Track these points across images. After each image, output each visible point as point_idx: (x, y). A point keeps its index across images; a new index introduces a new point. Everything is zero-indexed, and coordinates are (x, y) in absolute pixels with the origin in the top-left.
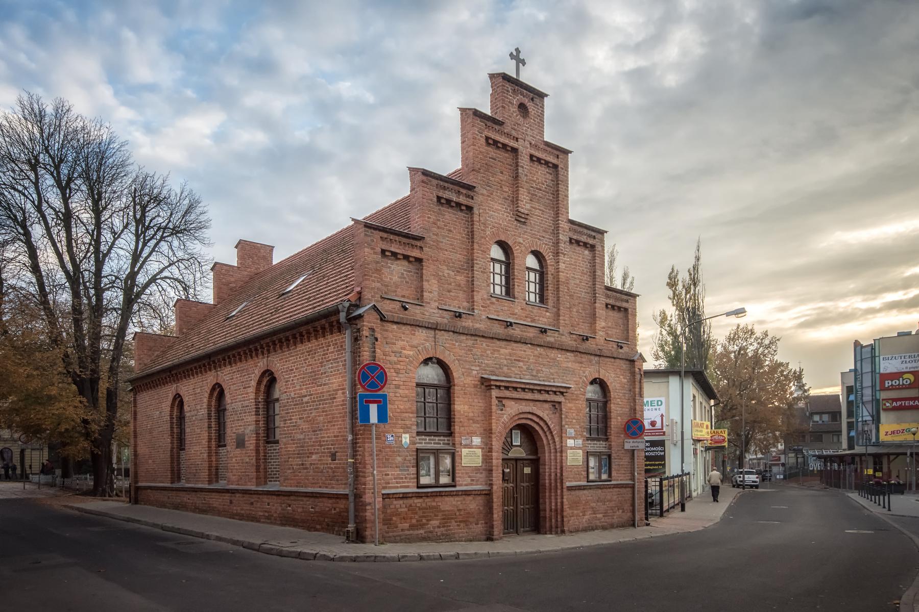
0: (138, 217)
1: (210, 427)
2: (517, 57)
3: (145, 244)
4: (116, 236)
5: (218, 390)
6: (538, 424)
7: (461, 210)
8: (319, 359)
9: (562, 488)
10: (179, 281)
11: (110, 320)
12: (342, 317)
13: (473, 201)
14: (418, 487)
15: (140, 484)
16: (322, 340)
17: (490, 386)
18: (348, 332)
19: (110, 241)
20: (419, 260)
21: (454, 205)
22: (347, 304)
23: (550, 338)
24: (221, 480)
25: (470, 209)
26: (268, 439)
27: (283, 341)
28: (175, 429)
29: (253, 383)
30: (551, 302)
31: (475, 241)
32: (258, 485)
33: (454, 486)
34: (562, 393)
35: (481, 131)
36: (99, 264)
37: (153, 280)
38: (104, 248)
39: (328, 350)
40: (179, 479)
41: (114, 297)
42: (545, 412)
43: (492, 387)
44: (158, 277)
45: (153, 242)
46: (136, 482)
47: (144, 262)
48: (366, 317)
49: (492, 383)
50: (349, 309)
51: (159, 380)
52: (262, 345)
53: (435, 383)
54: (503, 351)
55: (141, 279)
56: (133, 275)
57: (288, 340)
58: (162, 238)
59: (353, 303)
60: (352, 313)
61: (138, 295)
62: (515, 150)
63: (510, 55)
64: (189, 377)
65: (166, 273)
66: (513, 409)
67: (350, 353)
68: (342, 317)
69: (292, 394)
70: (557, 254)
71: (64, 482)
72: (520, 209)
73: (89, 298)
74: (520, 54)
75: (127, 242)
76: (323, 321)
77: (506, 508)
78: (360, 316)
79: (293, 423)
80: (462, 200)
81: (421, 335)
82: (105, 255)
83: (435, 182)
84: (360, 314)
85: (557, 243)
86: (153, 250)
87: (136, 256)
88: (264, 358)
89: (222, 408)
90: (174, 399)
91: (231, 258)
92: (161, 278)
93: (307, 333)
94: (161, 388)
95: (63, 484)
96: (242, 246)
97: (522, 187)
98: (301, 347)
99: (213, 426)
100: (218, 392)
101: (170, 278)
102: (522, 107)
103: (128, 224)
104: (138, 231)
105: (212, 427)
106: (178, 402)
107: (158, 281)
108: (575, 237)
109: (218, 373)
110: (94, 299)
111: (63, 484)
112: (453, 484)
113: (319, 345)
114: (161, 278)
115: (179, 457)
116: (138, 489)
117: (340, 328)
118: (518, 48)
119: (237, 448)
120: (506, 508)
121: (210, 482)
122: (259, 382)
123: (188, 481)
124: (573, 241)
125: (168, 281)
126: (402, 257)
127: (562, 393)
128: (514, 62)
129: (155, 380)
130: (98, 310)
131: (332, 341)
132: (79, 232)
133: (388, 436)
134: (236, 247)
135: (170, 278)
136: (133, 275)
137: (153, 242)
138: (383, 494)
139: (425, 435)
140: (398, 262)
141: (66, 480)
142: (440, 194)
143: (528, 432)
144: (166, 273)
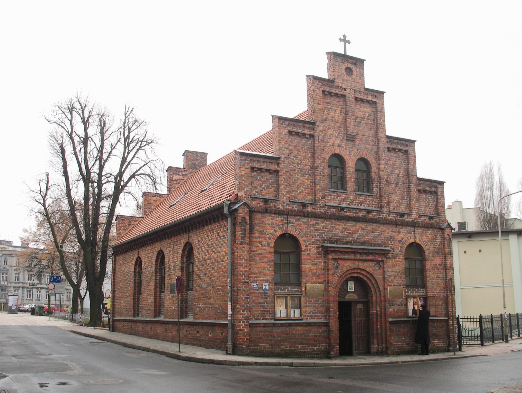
0: (126, 136)
1: (156, 279)
2: (344, 40)
3: (128, 153)
4: (113, 148)
5: (161, 254)
6: (366, 276)
7: (307, 138)
8: (216, 236)
9: (386, 323)
10: (149, 176)
11: (105, 205)
12: (226, 210)
13: (314, 131)
14: (275, 320)
15: (117, 318)
16: (217, 224)
17: (328, 251)
18: (229, 220)
19: (109, 150)
20: (277, 172)
21: (301, 135)
22: (228, 203)
23: (375, 216)
24: (162, 315)
25: (312, 136)
26: (189, 287)
27: (174, 231)
28: (137, 280)
29: (180, 251)
30: (376, 190)
31: (316, 156)
32: (134, 316)
33: (302, 320)
34: (384, 254)
35: (319, 88)
36: (101, 168)
37: (133, 176)
38: (105, 157)
39: (220, 230)
40: (138, 315)
41: (109, 188)
42: (369, 267)
43: (329, 252)
44: (136, 174)
45: (135, 151)
46: (113, 316)
47: (129, 164)
48: (240, 210)
49: (330, 249)
50: (230, 205)
51: (129, 248)
52: (185, 226)
53: (110, 282)
54: (337, 227)
55: (125, 177)
56: (121, 174)
57: (199, 223)
58: (140, 148)
59: (233, 201)
60: (232, 208)
61: (123, 187)
62: (344, 96)
63: (339, 39)
64: (146, 246)
65: (140, 172)
66: (346, 265)
67: (230, 233)
68: (226, 210)
69: (201, 258)
70: (378, 159)
71: (73, 316)
72: (348, 133)
73: (94, 189)
74: (346, 38)
75: (120, 149)
76: (217, 212)
77: (356, 335)
78: (236, 210)
79: (201, 277)
80: (307, 131)
81: (278, 220)
82: (106, 161)
83: (287, 122)
84: (236, 209)
85: (377, 152)
86: (134, 156)
87: (124, 160)
88: (186, 234)
89: (191, 261)
90: (158, 254)
91: (179, 163)
92: (139, 175)
93: (176, 231)
94: (130, 252)
95: (72, 318)
96: (187, 154)
97: (349, 119)
98: (206, 228)
99: (158, 278)
100: (161, 257)
101: (143, 174)
102: (349, 71)
103: (120, 138)
104: (126, 145)
105: (157, 279)
106: (139, 262)
107: (136, 177)
108: (391, 146)
109: (162, 243)
110: (96, 191)
111: (72, 318)
112: (301, 318)
113: (215, 227)
114: (139, 175)
115: (160, 297)
116: (114, 321)
117: (224, 217)
118: (344, 35)
119: (170, 293)
120: (356, 335)
121: (155, 316)
122: (184, 250)
123: (120, 315)
124: (390, 149)
125: (142, 176)
126: (265, 171)
127: (384, 254)
128: (342, 43)
129: (127, 248)
130: (99, 198)
131: (223, 224)
132: (91, 147)
133: (254, 285)
134: (183, 155)
135: (143, 174)
136: (121, 174)
137: (135, 151)
138: (250, 324)
139: (280, 285)
140: (263, 174)
141: (74, 315)
142: (291, 129)
143: (360, 283)
144: (140, 172)
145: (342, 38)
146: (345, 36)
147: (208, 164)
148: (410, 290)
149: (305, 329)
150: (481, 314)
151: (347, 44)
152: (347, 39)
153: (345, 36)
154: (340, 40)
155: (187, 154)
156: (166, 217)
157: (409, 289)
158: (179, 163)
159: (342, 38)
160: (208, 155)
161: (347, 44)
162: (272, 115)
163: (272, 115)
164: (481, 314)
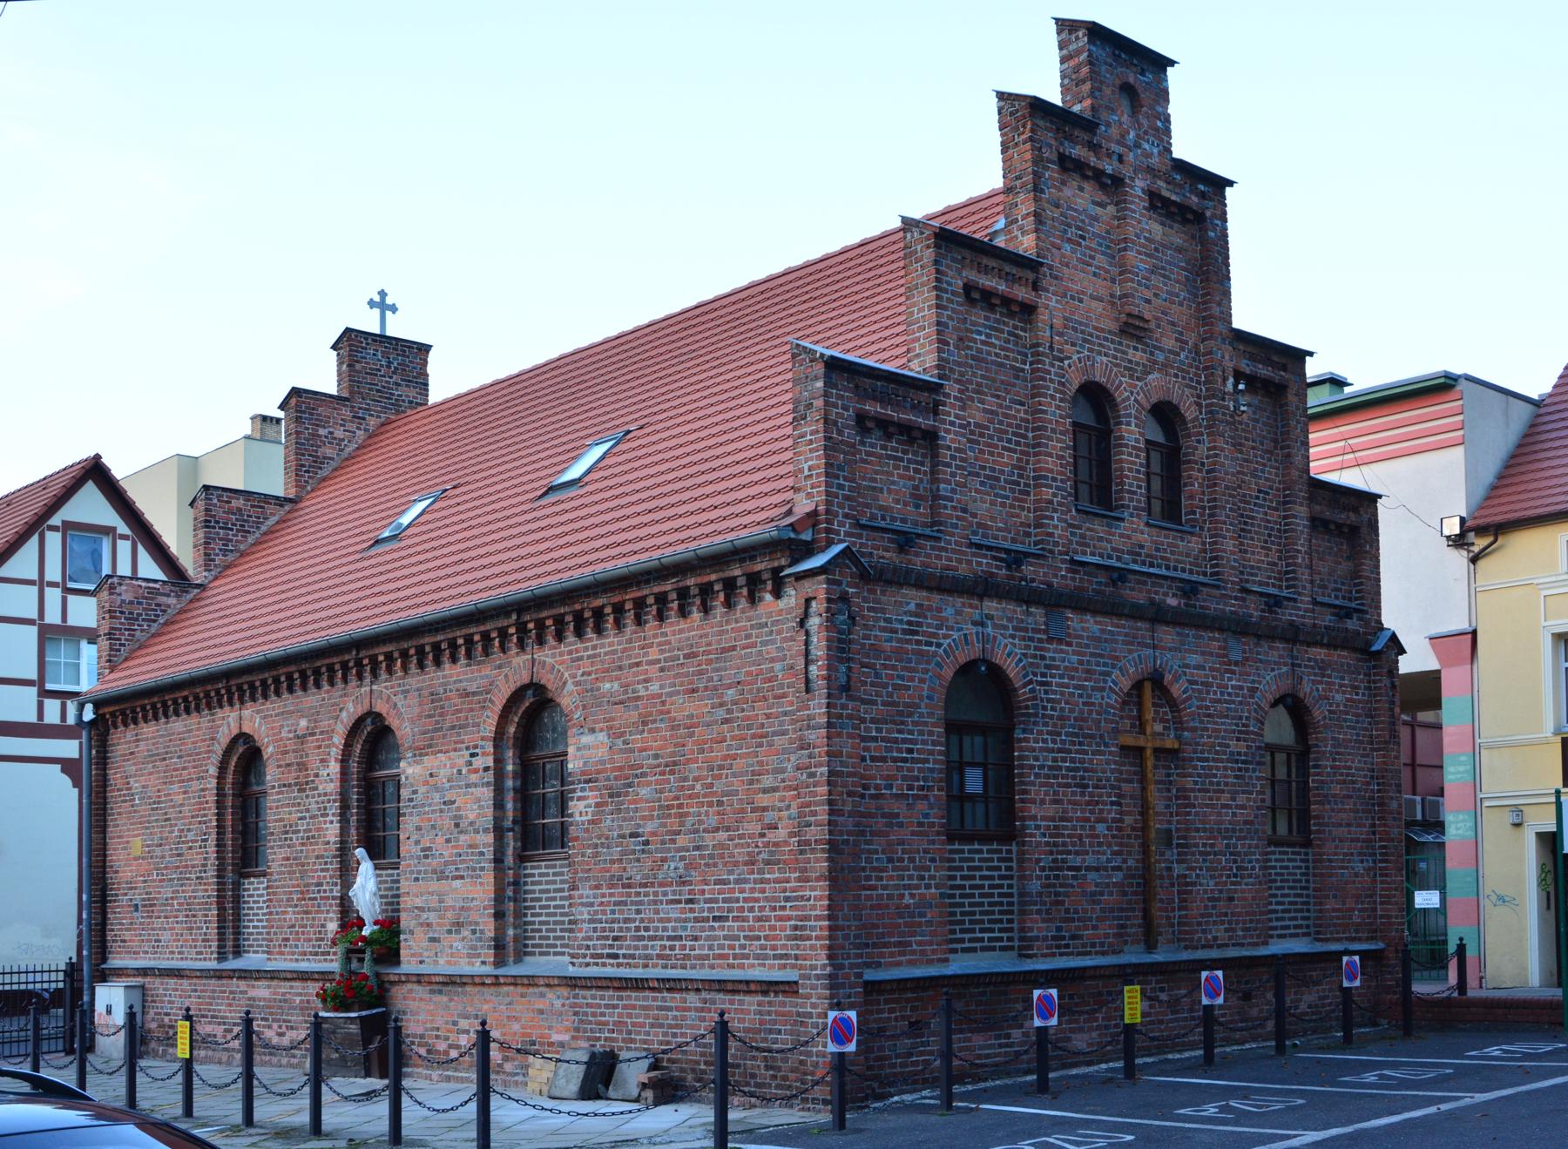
2: (382, 304)
91: (324, 377)
128: (377, 311)
134: (334, 347)
138: (867, 983)
145: (377, 298)
146: (383, 294)
147: (436, 394)
148: (981, 851)
149: (512, 920)
150: (1461, 939)
151: (388, 314)
152: (389, 301)
153: (383, 294)
154: (372, 304)
155: (351, 343)
156: (264, 597)
157: (976, 847)
158: (324, 377)
159: (377, 298)
160: (432, 354)
161: (388, 314)
162: (1057, 20)
163: (1057, 20)
164: (1461, 939)
